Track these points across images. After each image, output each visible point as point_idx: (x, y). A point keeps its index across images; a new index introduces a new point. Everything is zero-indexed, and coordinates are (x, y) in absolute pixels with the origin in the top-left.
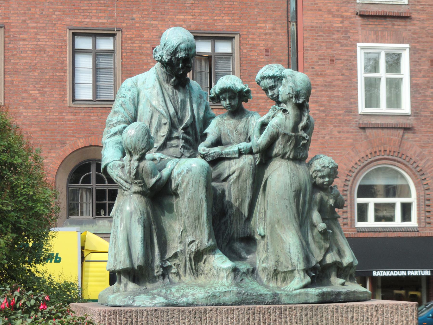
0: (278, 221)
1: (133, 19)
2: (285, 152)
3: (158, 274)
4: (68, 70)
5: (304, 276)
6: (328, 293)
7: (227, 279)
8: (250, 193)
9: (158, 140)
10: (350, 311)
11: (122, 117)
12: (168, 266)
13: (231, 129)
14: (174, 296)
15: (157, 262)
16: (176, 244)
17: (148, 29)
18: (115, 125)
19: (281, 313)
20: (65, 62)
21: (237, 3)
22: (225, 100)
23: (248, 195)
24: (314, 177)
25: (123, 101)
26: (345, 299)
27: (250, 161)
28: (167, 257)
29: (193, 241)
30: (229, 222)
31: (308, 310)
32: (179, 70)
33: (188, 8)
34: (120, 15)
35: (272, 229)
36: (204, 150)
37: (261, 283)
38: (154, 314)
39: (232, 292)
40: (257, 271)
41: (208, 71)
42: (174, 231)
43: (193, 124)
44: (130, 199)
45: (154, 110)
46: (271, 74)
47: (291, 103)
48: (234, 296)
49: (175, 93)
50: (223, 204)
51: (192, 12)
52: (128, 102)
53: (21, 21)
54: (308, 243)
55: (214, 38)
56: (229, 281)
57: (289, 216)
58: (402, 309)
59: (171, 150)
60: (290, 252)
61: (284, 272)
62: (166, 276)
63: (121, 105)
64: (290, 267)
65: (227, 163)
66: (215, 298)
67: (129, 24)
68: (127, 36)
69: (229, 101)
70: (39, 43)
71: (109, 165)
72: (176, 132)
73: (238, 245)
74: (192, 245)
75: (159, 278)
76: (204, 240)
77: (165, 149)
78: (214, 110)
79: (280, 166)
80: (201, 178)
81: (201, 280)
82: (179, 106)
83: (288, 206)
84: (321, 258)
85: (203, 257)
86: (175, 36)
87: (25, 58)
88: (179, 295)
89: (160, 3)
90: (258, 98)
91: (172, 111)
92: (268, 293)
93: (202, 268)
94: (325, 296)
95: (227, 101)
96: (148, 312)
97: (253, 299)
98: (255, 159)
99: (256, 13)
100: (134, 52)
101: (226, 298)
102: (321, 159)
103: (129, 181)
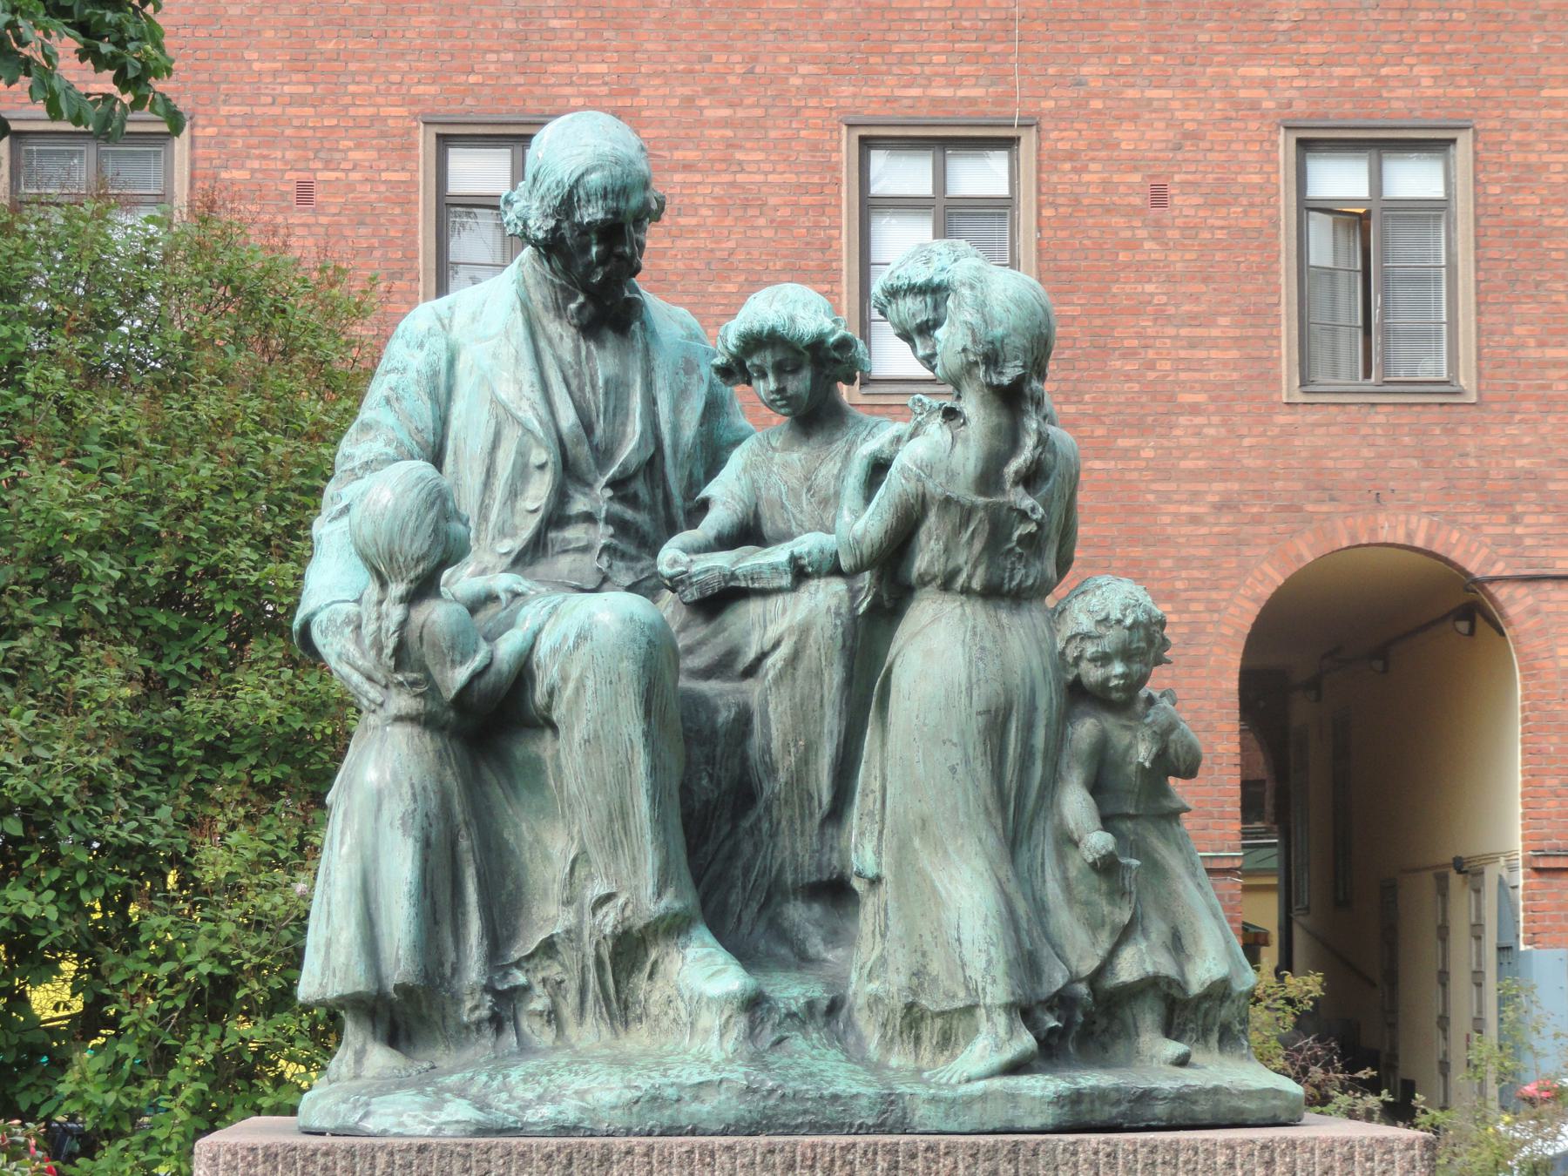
0: (924, 822)
1: (1079, 84)
2: (951, 566)
3: (477, 1014)
4: (844, 273)
5: (1011, 1031)
6: (1100, 1095)
7: (722, 1036)
8: (836, 721)
9: (515, 528)
10: (1164, 1163)
11: (388, 444)
12: (514, 989)
13: (795, 483)
14: (512, 1099)
15: (474, 971)
16: (553, 909)
17: (1135, 118)
18: (360, 474)
19: (896, 1168)
20: (834, 243)
21: (1463, 16)
22: (763, 375)
23: (830, 726)
24: (1070, 660)
25: (393, 384)
26: (1171, 1117)
27: (833, 602)
28: (515, 954)
29: (609, 897)
30: (765, 826)
31: (1000, 1156)
32: (590, 268)
33: (1281, 39)
34: (1033, 69)
35: (903, 847)
36: (675, 562)
37: (855, 1056)
38: (416, 1162)
39: (725, 1085)
40: (850, 1010)
41: (1359, 267)
42: (547, 858)
43: (652, 466)
44: (383, 740)
45: (503, 417)
46: (920, 280)
47: (976, 385)
48: (734, 1102)
49: (584, 353)
50: (744, 759)
51: (1297, 53)
52: (414, 388)
53: (676, 102)
54: (1040, 909)
55: (1380, 145)
56: (729, 1045)
57: (960, 804)
58: (1370, 1159)
59: (564, 564)
60: (959, 940)
61: (942, 1014)
62: (509, 1026)
63: (388, 401)
64: (962, 994)
65: (754, 608)
66: (660, 1108)
67: (1067, 103)
68: (1060, 145)
69: (778, 379)
70: (740, 178)
71: (317, 619)
72: (585, 494)
73: (798, 914)
74: (605, 909)
75: (479, 1030)
76: (643, 893)
77: (543, 561)
78: (1379, 409)
79: (936, 619)
80: (625, 663)
81: (637, 1039)
82: (597, 401)
83: (960, 769)
84: (1096, 963)
85: (646, 955)
86: (578, 145)
87: (692, 231)
88: (529, 1095)
89: (1180, 22)
90: (1544, 365)
91: (567, 418)
92: (863, 1090)
93: (642, 997)
94: (1084, 1107)
95: (771, 378)
96: (391, 1154)
97: (805, 1112)
98: (854, 594)
99: (1535, 49)
100: (1086, 201)
101: (704, 1109)
102: (1098, 592)
103: (379, 676)
